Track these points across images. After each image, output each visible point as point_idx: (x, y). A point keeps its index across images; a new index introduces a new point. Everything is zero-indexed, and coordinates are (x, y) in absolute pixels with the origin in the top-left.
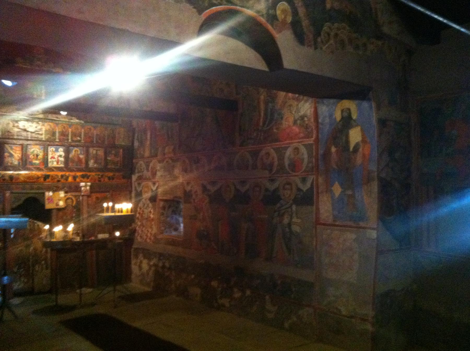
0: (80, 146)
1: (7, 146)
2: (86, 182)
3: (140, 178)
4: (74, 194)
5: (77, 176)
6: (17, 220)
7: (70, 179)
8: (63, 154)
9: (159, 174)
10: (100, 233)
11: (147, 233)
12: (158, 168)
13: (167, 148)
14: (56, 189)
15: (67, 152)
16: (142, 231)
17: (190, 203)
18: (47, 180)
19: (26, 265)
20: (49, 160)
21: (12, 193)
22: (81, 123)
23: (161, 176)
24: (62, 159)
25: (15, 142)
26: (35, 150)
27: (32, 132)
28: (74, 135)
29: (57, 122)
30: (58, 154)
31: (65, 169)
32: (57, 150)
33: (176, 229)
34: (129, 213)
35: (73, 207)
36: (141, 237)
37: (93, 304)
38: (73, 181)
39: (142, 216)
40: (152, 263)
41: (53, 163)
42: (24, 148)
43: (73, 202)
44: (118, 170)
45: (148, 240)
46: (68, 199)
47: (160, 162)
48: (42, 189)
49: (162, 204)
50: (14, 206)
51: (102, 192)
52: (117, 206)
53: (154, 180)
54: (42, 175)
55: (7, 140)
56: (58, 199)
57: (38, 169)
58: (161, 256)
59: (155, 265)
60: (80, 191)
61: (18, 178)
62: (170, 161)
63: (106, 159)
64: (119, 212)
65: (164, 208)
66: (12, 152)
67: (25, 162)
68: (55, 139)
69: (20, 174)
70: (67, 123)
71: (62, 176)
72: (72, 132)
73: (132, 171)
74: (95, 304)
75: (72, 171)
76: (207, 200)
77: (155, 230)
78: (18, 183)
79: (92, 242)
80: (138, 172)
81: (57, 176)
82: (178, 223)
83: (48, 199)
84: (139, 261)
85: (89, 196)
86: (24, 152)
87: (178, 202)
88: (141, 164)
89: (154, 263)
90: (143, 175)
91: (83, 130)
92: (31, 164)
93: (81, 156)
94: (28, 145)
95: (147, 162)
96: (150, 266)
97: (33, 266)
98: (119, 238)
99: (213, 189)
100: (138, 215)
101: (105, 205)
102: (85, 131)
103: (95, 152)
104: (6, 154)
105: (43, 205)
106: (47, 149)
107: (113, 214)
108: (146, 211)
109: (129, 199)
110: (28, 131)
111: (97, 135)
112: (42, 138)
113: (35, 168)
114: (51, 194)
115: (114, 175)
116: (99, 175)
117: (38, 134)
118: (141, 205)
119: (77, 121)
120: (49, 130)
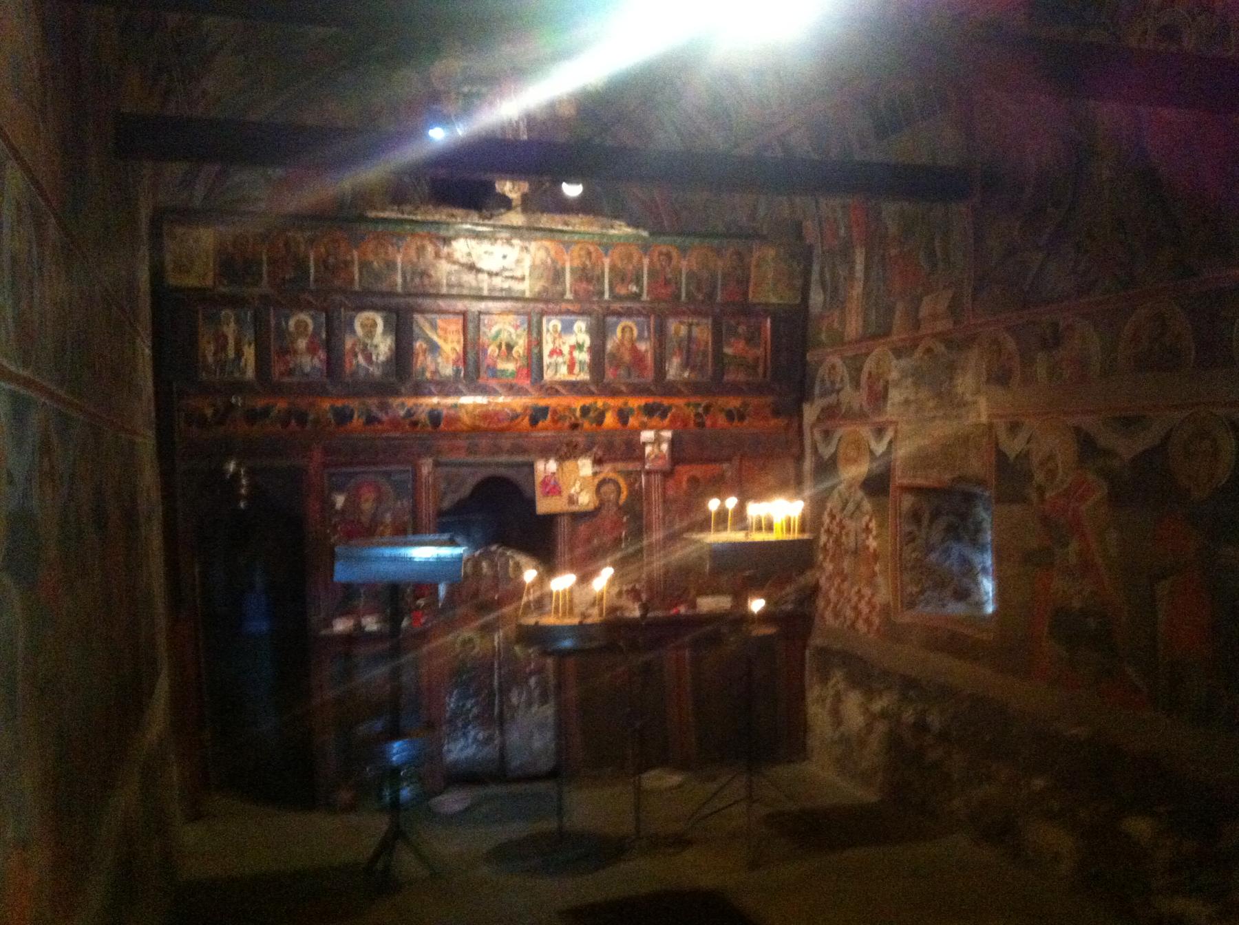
0: (639, 313)
1: (418, 317)
2: (658, 429)
3: (830, 413)
4: (620, 466)
5: (631, 411)
6: (447, 552)
7: (610, 420)
8: (586, 339)
9: (895, 396)
10: (706, 594)
11: (858, 600)
12: (894, 375)
13: (926, 299)
14: (566, 452)
15: (599, 333)
16: (840, 592)
17: (1025, 500)
18: (540, 424)
19: (487, 686)
20: (546, 360)
21: (437, 464)
22: (638, 237)
23: (907, 402)
24: (583, 356)
25: (442, 304)
26: (503, 327)
27: (490, 274)
28: (619, 276)
29: (566, 237)
30: (571, 340)
31: (593, 388)
32: (568, 328)
33: (965, 594)
34: (795, 535)
35: (620, 508)
36: (837, 615)
37: (681, 842)
38: (619, 425)
39: (837, 542)
40: (877, 706)
41: (556, 371)
42: (470, 325)
43: (619, 492)
44: (759, 389)
45: (861, 626)
46: (603, 482)
47: (898, 353)
48: (525, 451)
49: (907, 502)
50: (446, 504)
51: (710, 460)
52: (755, 510)
53: (877, 419)
54: (526, 408)
55: (420, 301)
56: (573, 483)
57: (512, 389)
58: (909, 686)
59: (884, 714)
60: (642, 458)
61: (457, 419)
62: (940, 348)
63: (719, 356)
64: (759, 529)
65: (916, 516)
66: (435, 338)
67: (473, 370)
68: (563, 294)
69: (463, 406)
70: (596, 239)
71: (585, 411)
72: (613, 268)
73: (803, 394)
74: (690, 843)
75: (615, 393)
76: (1101, 491)
77: (884, 595)
78: (455, 434)
79: (679, 625)
80: (823, 395)
81: (570, 409)
82: (970, 572)
83: (545, 483)
84: (832, 692)
85: (667, 475)
86: (470, 335)
87: (969, 498)
88: (831, 364)
89: (883, 709)
90: (839, 403)
91: (646, 261)
92: (495, 373)
93: (643, 346)
94: (480, 313)
95: (855, 357)
96: (872, 718)
97: (504, 691)
98: (764, 617)
99: (1127, 447)
100: (823, 538)
101: (713, 505)
102: (651, 262)
103: (683, 330)
104: (419, 345)
105: (531, 503)
106: (540, 323)
107: (739, 537)
108: (851, 525)
109: (791, 485)
110: (479, 271)
111: (691, 275)
112: (524, 292)
113: (504, 386)
114: (552, 466)
115: (745, 405)
116: (698, 405)
117: (512, 278)
118: (833, 503)
119: (629, 230)
120: (544, 263)
